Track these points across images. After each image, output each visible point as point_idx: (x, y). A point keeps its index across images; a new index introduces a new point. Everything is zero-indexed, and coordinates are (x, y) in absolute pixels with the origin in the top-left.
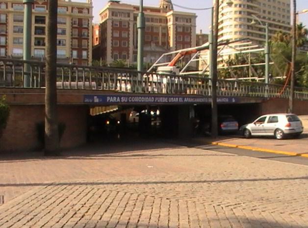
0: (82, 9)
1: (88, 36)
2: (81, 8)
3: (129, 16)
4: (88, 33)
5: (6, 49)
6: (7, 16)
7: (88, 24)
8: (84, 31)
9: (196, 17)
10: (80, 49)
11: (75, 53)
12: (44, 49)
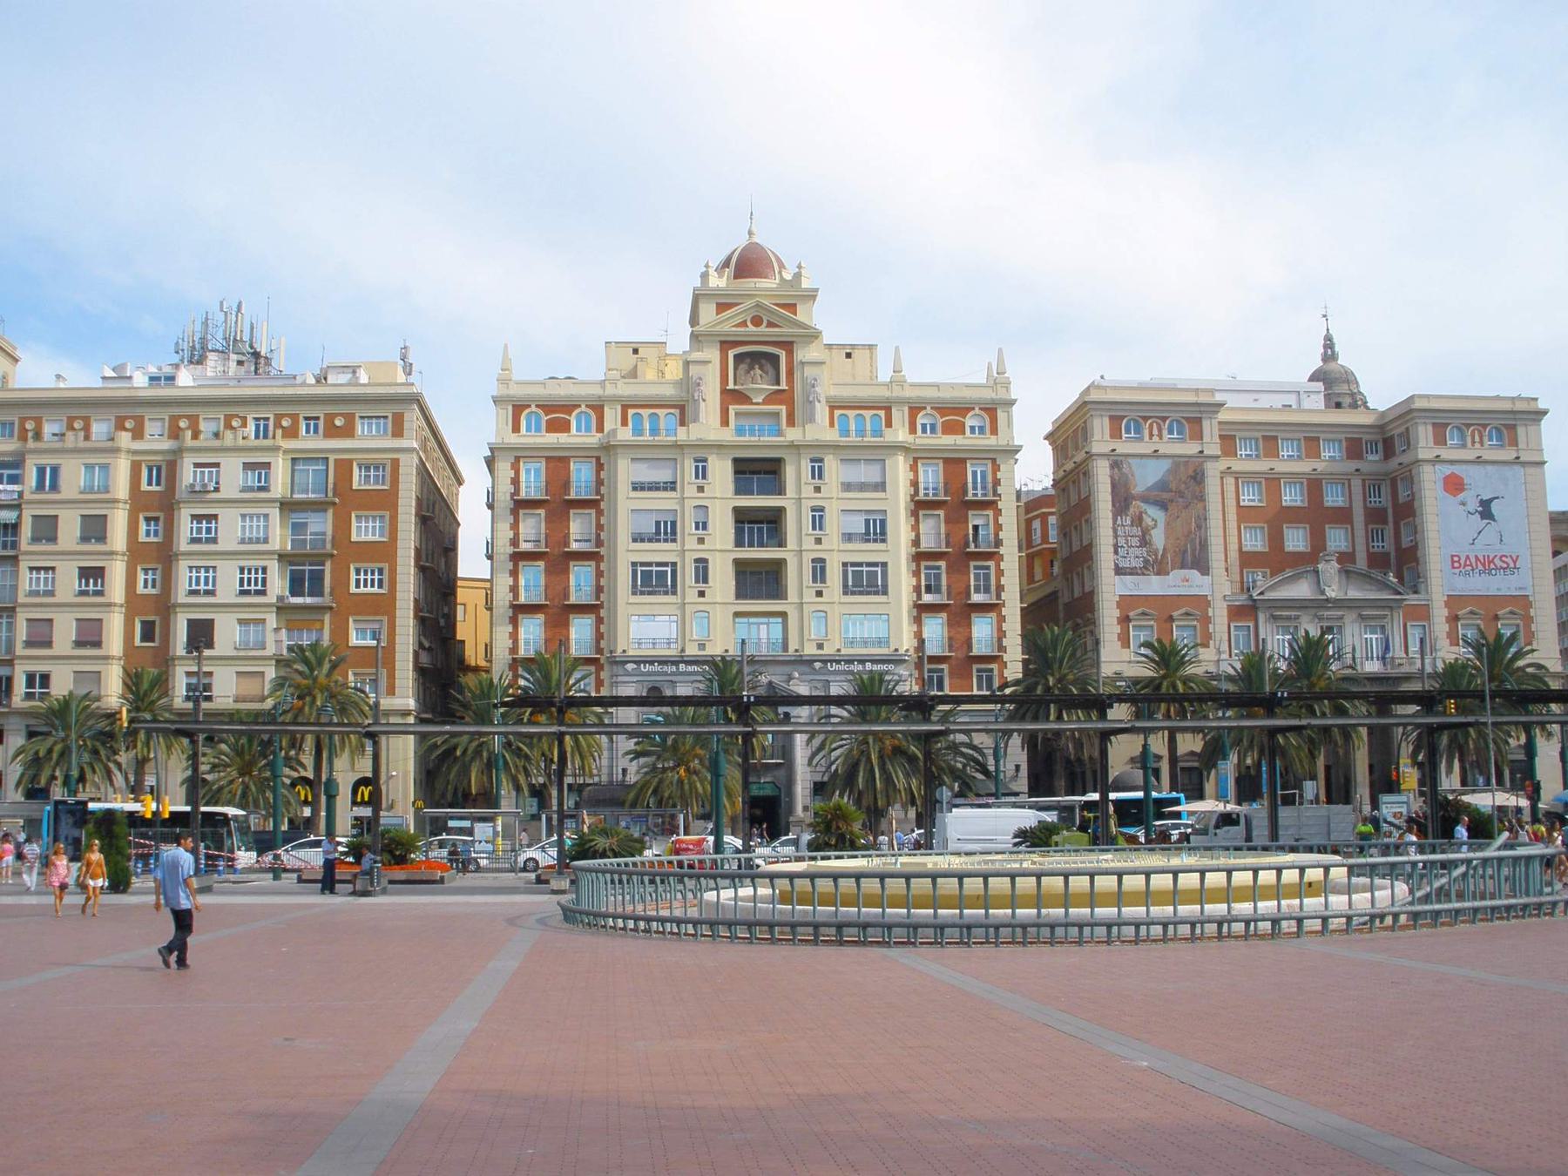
0: (569, 408)
1: (998, 543)
2: (952, 413)
3: (1198, 436)
4: (999, 527)
5: (599, 621)
6: (600, 467)
7: (997, 482)
8: (975, 519)
9: (1012, 403)
10: (961, 613)
11: (935, 629)
12: (783, 615)
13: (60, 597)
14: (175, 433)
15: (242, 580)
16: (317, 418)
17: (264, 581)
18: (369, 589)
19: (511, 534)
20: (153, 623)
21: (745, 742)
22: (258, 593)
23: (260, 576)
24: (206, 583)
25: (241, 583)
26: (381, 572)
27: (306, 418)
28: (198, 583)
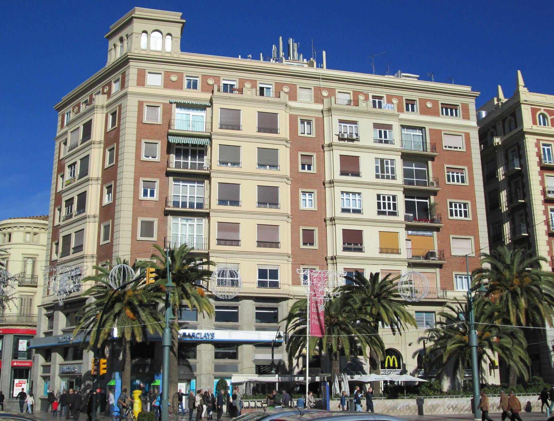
13: (365, 215)
14: (319, 99)
15: (379, 204)
16: (381, 98)
17: (394, 205)
18: (459, 217)
19: (541, 188)
20: (152, 223)
21: (421, 365)
22: (391, 214)
23: (391, 202)
24: (389, 208)
25: (379, 207)
27: (374, 97)
28: (384, 208)
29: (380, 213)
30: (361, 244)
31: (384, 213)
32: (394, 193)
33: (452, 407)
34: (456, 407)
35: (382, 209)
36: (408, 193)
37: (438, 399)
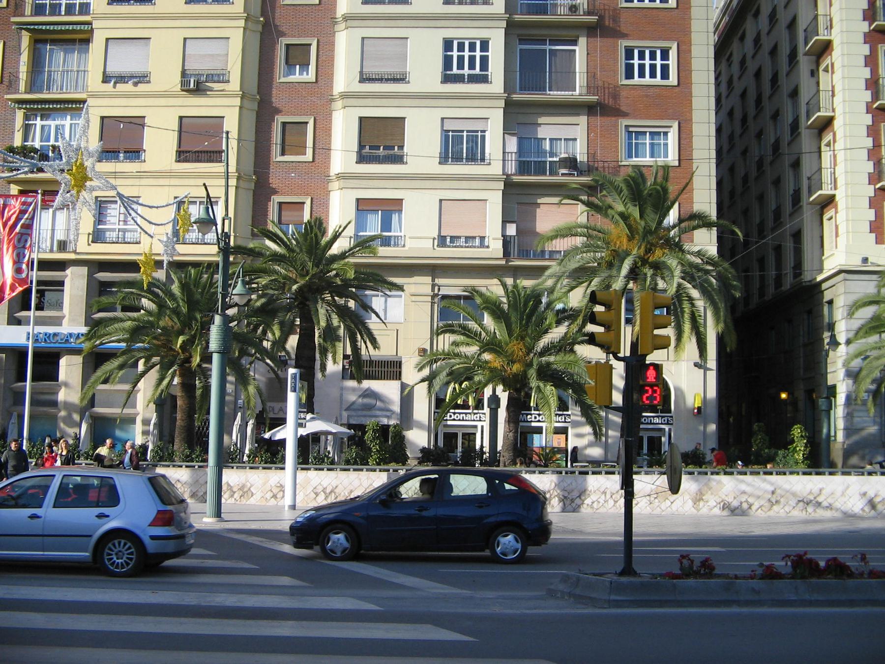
22: (473, 79)
24: (472, 66)
26: (665, 55)
28: (461, 66)
29: (447, 79)
30: (401, 147)
31: (459, 79)
32: (484, 34)
33: (324, 491)
34: (331, 492)
35: (455, 71)
36: (512, 28)
37: (325, 472)
